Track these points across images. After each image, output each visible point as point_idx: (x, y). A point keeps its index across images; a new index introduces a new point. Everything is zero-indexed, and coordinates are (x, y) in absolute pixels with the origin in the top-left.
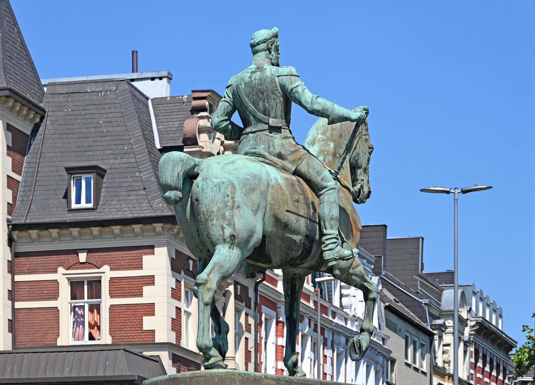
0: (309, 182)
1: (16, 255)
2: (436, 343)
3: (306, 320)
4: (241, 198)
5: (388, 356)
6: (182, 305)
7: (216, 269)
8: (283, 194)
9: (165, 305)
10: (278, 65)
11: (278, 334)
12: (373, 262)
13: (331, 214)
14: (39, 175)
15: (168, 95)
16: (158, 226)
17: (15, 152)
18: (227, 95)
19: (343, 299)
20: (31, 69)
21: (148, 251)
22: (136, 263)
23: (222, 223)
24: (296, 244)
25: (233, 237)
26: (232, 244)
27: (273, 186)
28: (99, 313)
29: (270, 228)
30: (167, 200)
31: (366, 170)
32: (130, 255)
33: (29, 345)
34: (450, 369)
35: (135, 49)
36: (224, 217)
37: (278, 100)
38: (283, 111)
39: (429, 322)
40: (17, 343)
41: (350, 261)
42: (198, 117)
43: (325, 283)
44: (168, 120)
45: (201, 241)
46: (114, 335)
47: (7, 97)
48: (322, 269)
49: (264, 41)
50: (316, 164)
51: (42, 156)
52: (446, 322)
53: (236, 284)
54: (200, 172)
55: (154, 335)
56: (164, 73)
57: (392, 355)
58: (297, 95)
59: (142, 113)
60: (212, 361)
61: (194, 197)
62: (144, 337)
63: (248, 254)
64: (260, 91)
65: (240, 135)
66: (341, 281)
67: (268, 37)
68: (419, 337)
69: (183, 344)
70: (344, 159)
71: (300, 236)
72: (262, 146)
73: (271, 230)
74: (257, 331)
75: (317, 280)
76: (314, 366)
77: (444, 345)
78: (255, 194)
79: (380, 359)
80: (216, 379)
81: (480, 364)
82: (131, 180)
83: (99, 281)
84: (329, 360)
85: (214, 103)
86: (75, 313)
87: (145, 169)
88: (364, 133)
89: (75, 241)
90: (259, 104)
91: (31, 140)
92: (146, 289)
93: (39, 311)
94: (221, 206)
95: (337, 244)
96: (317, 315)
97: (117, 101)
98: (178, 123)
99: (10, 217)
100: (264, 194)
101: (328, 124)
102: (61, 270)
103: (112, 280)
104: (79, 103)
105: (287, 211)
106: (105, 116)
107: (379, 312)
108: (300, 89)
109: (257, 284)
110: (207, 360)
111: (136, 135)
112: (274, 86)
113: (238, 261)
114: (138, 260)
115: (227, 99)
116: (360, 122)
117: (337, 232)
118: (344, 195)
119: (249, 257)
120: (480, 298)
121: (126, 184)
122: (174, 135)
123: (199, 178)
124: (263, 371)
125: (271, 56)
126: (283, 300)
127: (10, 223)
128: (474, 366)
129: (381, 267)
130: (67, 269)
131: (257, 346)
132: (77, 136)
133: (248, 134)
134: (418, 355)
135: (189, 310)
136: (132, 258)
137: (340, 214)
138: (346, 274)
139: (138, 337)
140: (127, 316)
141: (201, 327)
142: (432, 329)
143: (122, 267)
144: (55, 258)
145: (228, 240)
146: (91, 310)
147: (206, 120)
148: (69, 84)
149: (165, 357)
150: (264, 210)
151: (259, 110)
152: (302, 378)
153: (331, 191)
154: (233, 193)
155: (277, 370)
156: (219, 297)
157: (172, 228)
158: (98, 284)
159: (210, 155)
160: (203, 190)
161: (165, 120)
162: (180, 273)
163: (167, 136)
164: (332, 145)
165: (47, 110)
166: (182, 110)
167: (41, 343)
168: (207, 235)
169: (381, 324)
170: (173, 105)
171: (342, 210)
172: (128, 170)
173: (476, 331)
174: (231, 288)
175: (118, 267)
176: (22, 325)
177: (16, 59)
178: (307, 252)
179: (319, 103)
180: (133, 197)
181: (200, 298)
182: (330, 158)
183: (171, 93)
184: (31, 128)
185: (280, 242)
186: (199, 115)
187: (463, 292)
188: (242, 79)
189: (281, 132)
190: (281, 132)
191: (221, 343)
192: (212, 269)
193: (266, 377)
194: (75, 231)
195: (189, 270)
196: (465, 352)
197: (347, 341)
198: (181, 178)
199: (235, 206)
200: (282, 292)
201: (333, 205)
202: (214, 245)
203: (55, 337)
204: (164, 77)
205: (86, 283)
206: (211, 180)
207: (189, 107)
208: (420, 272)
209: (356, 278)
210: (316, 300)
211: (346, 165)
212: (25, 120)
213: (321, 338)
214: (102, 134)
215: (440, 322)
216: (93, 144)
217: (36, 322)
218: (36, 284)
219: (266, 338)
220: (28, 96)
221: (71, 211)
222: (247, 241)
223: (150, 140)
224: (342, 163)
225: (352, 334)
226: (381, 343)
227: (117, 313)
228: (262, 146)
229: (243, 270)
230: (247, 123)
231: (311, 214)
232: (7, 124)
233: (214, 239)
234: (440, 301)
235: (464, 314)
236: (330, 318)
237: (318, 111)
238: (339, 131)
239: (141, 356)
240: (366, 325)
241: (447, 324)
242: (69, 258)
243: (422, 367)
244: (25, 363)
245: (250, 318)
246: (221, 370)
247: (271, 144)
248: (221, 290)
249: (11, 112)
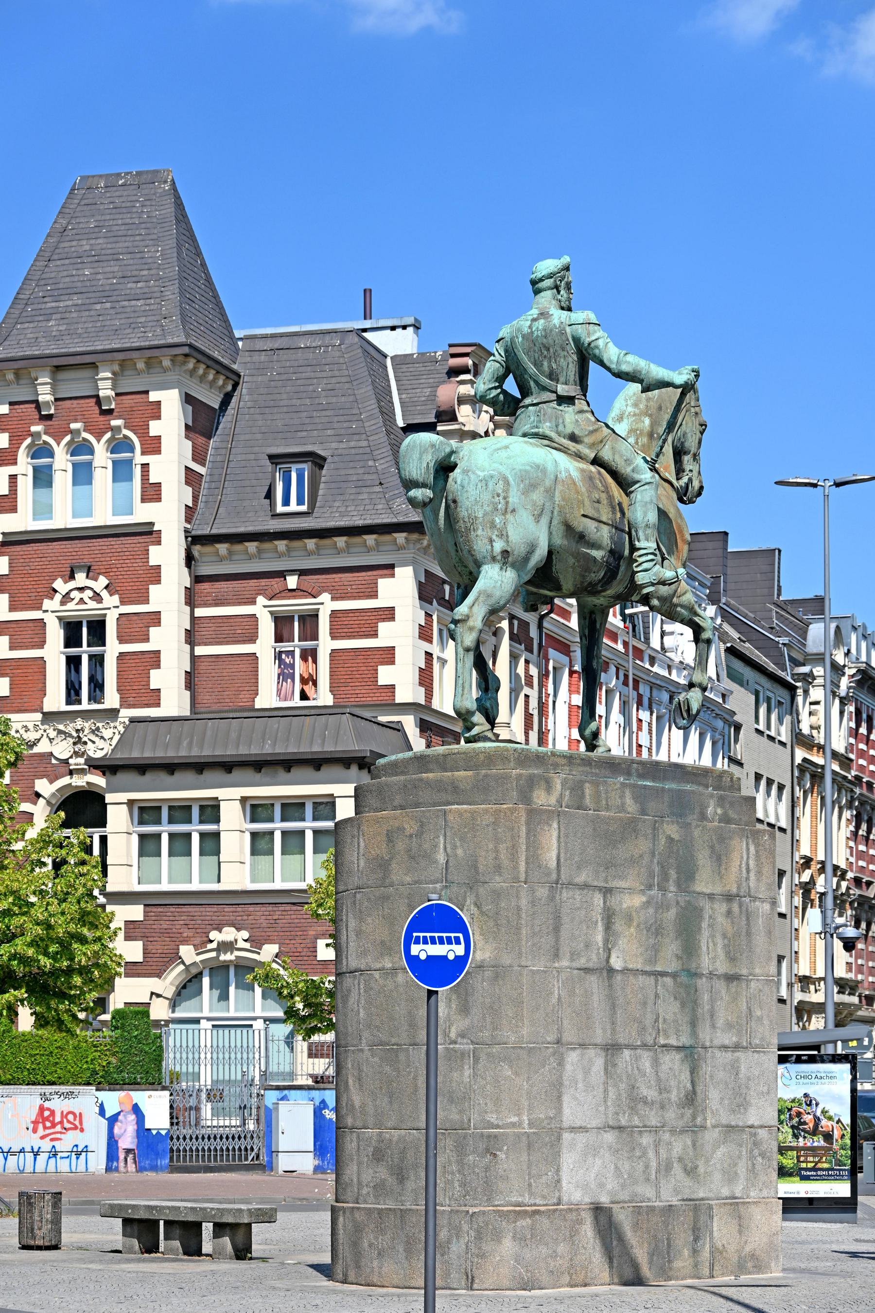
0: (614, 474)
1: (198, 579)
2: (800, 699)
3: (613, 669)
5: (730, 720)
6: (434, 648)
7: (481, 599)
8: (578, 492)
9: (410, 648)
10: (569, 309)
11: (572, 689)
12: (709, 584)
13: (646, 519)
14: (231, 465)
15: (415, 351)
16: (401, 537)
17: (196, 433)
18: (498, 351)
19: (665, 638)
20: (220, 317)
21: (385, 572)
22: (369, 590)
23: (490, 534)
25: (505, 553)
26: (505, 563)
27: (563, 481)
28: (315, 661)
29: (559, 541)
30: (412, 501)
31: (695, 457)
32: (360, 578)
33: (215, 707)
34: (820, 738)
35: (368, 287)
36: (493, 525)
37: (570, 360)
38: (577, 375)
39: (789, 670)
40: (197, 706)
41: (673, 586)
42: (458, 382)
43: (640, 616)
44: (415, 386)
45: (460, 559)
46: (335, 693)
47: (186, 355)
48: (633, 598)
49: (550, 276)
50: (625, 448)
51: (235, 439)
52: (814, 670)
53: (512, 617)
54: (458, 462)
55: (394, 692)
56: (410, 320)
57: (736, 718)
58: (597, 352)
59: (378, 377)
60: (475, 731)
61: (450, 498)
62: (378, 695)
63: (527, 578)
64: (545, 346)
65: (517, 409)
66: (662, 615)
67: (556, 270)
68: (775, 691)
69: (436, 704)
70: (665, 441)
72: (548, 424)
74: (541, 685)
75: (628, 611)
76: (624, 735)
77: (811, 704)
79: (720, 724)
80: (482, 757)
81: (863, 730)
82: (361, 471)
83: (315, 616)
84: (645, 726)
85: (480, 361)
86: (281, 662)
87: (382, 456)
88: (693, 404)
89: (282, 559)
90: (542, 364)
91: (219, 416)
92: (383, 627)
93: (230, 659)
94: (488, 509)
95: (654, 562)
96: (628, 662)
97: (342, 360)
98: (429, 390)
99: (188, 526)
100: (550, 492)
101: (642, 392)
102: (261, 600)
103: (334, 614)
104: (288, 364)
105: (584, 516)
106: (325, 381)
107: (718, 657)
108: (601, 343)
109: (542, 618)
110: (469, 729)
111: (369, 408)
112: (564, 338)
113: (513, 588)
114: (371, 586)
115: (498, 357)
116: (687, 388)
117: (655, 546)
118: (664, 493)
119: (529, 582)
120: (863, 635)
121: (355, 478)
122: (423, 407)
123: (457, 471)
124: (550, 746)
125: (559, 297)
126: (579, 640)
127: (188, 534)
128: (854, 733)
129: (720, 592)
130: (270, 599)
131: (542, 707)
132: (285, 409)
133: (527, 406)
134: (774, 717)
135: (443, 656)
136: (363, 582)
137: (659, 519)
138: (668, 604)
139: (371, 695)
140: (356, 665)
141: (460, 682)
142: (794, 680)
143: (349, 595)
144: (253, 583)
145: (499, 557)
146: (304, 658)
147: (469, 385)
148: (273, 336)
149: (409, 723)
150: (550, 515)
151: (542, 373)
152: (605, 754)
153: (646, 487)
154: (506, 491)
155: (570, 741)
156: (487, 638)
157: (420, 540)
158: (314, 619)
159: (474, 435)
160: (463, 487)
161: (410, 387)
162: (431, 603)
163: (413, 408)
164: (647, 421)
165: (242, 374)
166: (435, 372)
167: (231, 704)
168: (469, 551)
169: (720, 673)
170: (421, 365)
171: (662, 514)
172: (358, 457)
173: (858, 682)
174: (505, 624)
175: (343, 595)
176: (205, 679)
177: (199, 303)
178: (611, 574)
179: (629, 363)
180: (365, 496)
181: (459, 641)
182: (645, 440)
183: (419, 345)
184: (220, 400)
185: (573, 560)
186: (458, 379)
187: (838, 627)
188: (519, 330)
189: (574, 404)
190: (574, 404)
191: (488, 705)
192: (476, 600)
193: (553, 754)
194: (281, 545)
195: (444, 598)
196: (842, 713)
197: (671, 698)
198: (432, 471)
199: (509, 510)
200: (577, 628)
201: (649, 506)
202: (478, 565)
203: (252, 696)
204: (410, 326)
205: (296, 618)
206: (474, 473)
207: (444, 367)
208: (775, 598)
209: (683, 611)
210: (627, 640)
211: (668, 449)
212: (211, 388)
213: (633, 694)
214: (321, 407)
215: (805, 669)
216: (307, 421)
217: (224, 674)
218: (225, 621)
219: (555, 695)
220: (216, 355)
221: (276, 516)
222: (526, 559)
223: (388, 414)
224: (662, 447)
225: (678, 688)
226: (720, 701)
227: (341, 662)
228: (548, 424)
229: (521, 599)
230: (525, 391)
231: (618, 520)
232: (186, 393)
233: (479, 557)
234: (805, 639)
235: (840, 659)
236: (647, 666)
237: (627, 374)
238: (657, 401)
239: (374, 722)
240: (697, 678)
241: (816, 673)
242: (273, 583)
243: (779, 735)
244: (209, 733)
245: (531, 666)
246: (488, 744)
247: (561, 421)
248: (489, 627)
249: (191, 377)
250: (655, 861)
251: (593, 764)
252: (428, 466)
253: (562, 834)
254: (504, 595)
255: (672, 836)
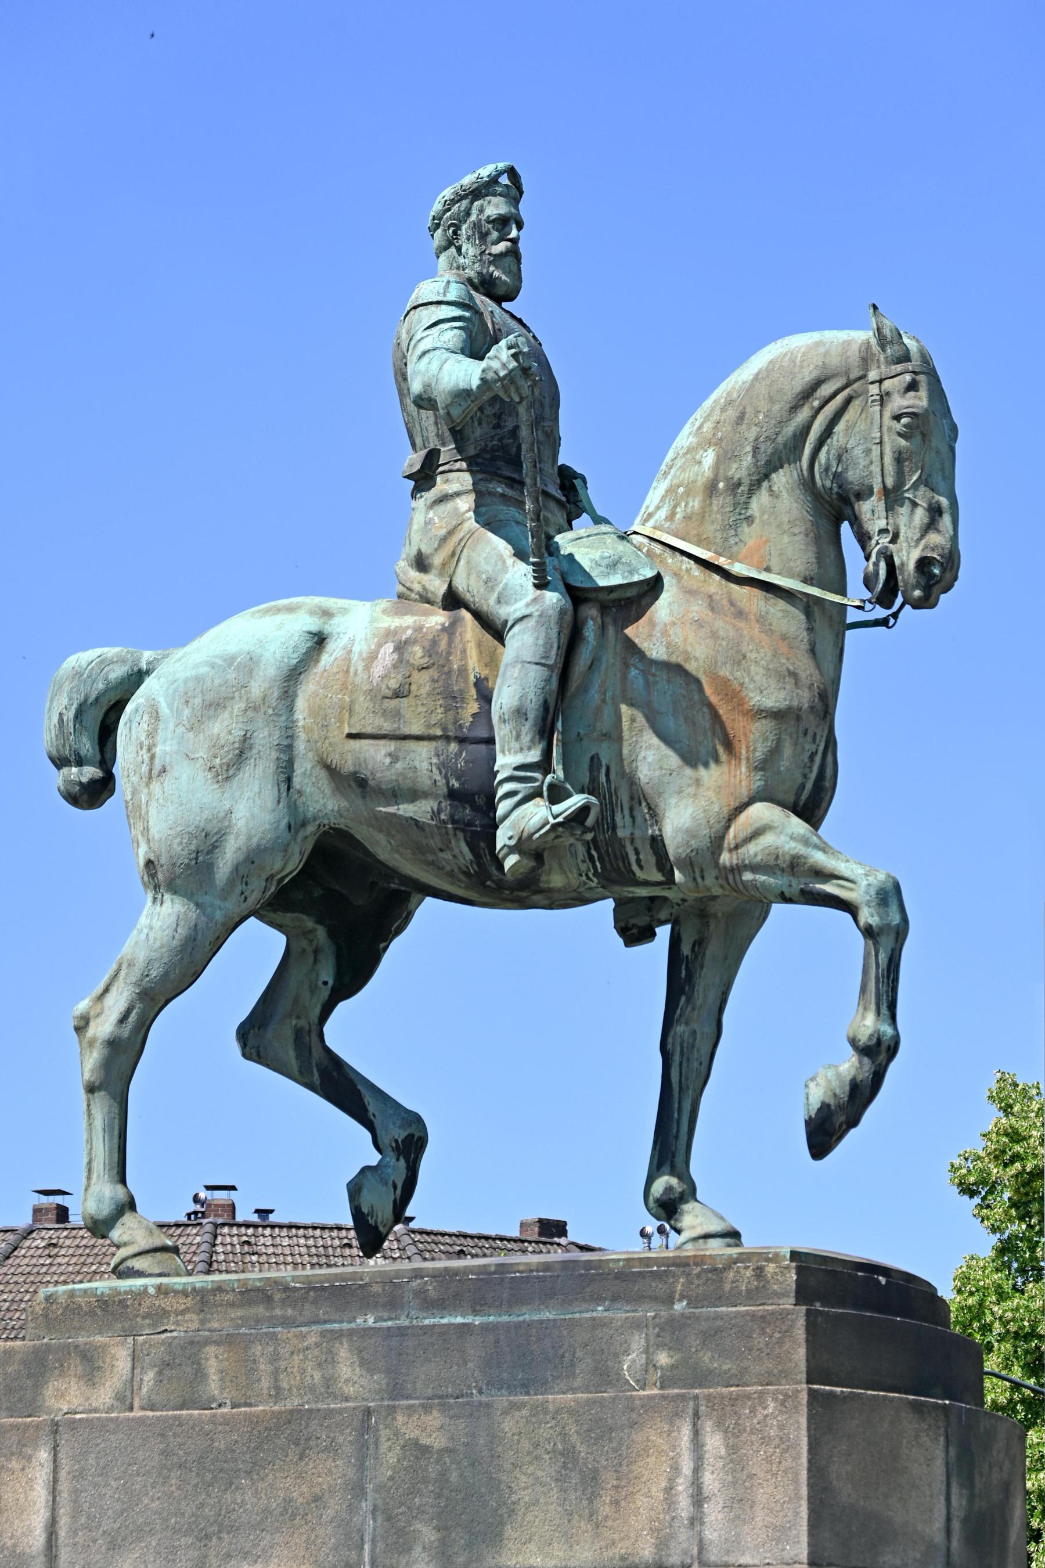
4: (174, 742)
24: (423, 830)
26: (156, 887)
71: (424, 802)
73: (336, 808)
78: (226, 715)
105: (350, 736)
250: (366, 1506)
251: (277, 1297)
252: (61, 720)
253: (63, 1474)
254: (154, 955)
255: (424, 1441)
